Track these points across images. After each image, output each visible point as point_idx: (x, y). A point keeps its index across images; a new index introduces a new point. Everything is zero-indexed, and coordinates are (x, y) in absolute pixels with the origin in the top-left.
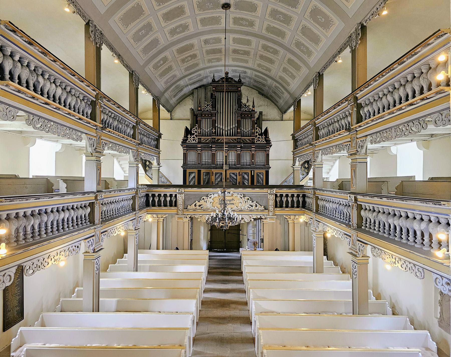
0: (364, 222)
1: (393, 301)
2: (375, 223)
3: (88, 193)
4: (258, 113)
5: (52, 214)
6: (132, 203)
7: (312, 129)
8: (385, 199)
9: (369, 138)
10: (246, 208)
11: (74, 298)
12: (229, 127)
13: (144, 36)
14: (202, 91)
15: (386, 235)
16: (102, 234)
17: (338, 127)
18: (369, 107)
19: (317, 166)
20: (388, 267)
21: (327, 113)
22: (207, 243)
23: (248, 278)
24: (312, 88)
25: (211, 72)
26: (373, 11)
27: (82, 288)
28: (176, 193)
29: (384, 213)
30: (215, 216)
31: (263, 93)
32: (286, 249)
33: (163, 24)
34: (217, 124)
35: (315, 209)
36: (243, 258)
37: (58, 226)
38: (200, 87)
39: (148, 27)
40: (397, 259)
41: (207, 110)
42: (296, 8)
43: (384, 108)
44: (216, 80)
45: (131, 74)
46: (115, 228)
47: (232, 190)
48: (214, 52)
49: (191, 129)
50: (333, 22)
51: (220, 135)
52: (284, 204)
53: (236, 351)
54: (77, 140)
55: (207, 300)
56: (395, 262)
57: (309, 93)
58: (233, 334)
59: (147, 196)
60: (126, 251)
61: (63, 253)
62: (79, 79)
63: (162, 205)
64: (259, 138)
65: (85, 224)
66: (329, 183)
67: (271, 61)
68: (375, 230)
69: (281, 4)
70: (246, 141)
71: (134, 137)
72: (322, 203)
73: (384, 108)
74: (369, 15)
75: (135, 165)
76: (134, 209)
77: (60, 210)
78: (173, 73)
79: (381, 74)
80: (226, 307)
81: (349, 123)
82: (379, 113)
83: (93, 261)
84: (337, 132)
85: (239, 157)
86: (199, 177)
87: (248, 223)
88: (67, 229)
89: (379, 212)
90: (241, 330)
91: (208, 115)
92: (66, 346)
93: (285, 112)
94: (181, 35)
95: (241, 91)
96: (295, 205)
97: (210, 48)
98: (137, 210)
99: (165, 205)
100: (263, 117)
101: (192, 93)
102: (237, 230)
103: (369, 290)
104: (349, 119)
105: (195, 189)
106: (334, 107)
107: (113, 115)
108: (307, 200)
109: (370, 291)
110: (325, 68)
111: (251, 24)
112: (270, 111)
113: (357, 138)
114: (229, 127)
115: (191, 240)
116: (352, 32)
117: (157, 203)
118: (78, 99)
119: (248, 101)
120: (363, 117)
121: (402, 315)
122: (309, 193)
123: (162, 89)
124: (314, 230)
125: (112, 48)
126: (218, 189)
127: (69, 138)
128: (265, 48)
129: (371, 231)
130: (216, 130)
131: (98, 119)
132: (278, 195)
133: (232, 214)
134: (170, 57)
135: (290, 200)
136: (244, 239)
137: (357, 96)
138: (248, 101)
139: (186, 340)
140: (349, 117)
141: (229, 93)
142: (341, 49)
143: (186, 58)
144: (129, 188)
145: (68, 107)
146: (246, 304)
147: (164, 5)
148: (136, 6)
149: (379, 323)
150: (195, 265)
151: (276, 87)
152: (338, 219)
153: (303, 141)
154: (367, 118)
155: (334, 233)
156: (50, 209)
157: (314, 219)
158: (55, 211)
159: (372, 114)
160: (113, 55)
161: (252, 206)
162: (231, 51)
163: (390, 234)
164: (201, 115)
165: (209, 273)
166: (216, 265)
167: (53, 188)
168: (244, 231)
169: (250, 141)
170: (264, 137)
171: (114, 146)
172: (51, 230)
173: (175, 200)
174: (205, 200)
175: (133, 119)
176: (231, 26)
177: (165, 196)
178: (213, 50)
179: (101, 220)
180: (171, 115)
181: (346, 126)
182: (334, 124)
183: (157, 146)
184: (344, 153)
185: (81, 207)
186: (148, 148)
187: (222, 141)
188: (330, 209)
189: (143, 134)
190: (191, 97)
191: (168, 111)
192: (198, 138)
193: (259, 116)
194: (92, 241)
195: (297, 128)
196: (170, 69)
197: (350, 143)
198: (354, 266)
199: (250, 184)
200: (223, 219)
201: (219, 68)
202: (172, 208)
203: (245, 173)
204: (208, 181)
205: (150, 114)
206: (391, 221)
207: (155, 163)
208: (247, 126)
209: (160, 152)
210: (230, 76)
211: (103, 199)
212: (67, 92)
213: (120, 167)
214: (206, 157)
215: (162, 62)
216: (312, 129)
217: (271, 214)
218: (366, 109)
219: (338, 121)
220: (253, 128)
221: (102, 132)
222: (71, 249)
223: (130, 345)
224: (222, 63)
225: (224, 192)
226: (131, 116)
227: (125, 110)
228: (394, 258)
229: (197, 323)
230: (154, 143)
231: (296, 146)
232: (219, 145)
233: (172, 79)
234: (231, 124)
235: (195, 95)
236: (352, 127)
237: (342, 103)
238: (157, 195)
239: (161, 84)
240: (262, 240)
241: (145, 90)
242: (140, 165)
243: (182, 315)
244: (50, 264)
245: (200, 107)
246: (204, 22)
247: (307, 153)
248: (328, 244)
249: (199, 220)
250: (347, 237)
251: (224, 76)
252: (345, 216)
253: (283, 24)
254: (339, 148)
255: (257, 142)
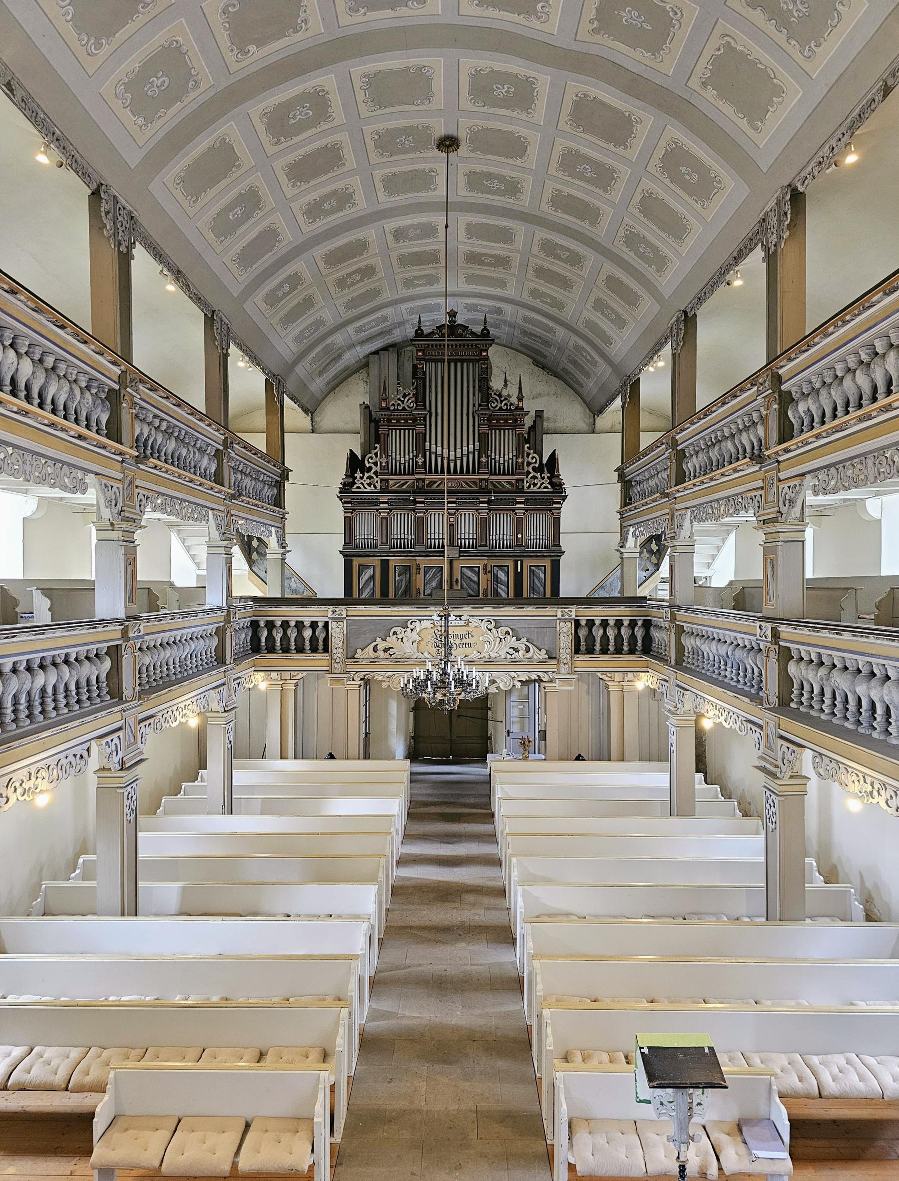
0: (796, 692)
1: (869, 885)
2: (822, 693)
3: (105, 622)
4: (532, 413)
5: (14, 678)
6: (215, 644)
7: (667, 455)
8: (847, 636)
9: (809, 481)
10: (503, 654)
11: (75, 881)
12: (459, 451)
13: (240, 222)
14: (390, 359)
15: (849, 725)
16: (142, 725)
17: (733, 450)
18: (810, 401)
19: (679, 549)
20: (854, 806)
21: (706, 415)
22: (406, 741)
23: (507, 830)
24: (667, 350)
25: (411, 312)
26: (821, 154)
27: (93, 857)
28: (326, 619)
29: (846, 668)
30: (422, 677)
31: (543, 364)
32: (603, 755)
33: (290, 192)
34: (427, 444)
35: (673, 656)
36: (496, 779)
37: (30, 707)
38: (385, 349)
39: (251, 201)
40: (877, 786)
41: (404, 409)
42: (626, 148)
43: (847, 404)
44: (426, 330)
45: (210, 320)
46: (175, 708)
47: (466, 611)
48: (420, 259)
49: (364, 457)
50: (720, 182)
51: (436, 472)
52: (598, 644)
53: (478, 1012)
54: (74, 490)
55: (408, 883)
56: (871, 793)
57: (661, 364)
58: (468, 968)
59: (254, 625)
60: (203, 765)
61: (43, 773)
62: (75, 335)
63: (293, 647)
64: (534, 477)
65: (99, 700)
66: (711, 591)
67: (565, 283)
68: (822, 710)
69: (587, 137)
70: (503, 486)
71: (218, 478)
72: (693, 642)
73: (847, 404)
74: (812, 164)
75: (222, 550)
76: (220, 660)
77: (36, 666)
78: (317, 316)
79: (839, 317)
80: (454, 902)
81: (760, 441)
82: (835, 416)
83: (119, 791)
84: (731, 463)
85: (484, 526)
86: (384, 578)
87: (508, 693)
88: (54, 714)
89: (834, 666)
90: (485, 957)
91: (406, 421)
92: (57, 1002)
93: (601, 411)
94: (333, 217)
95: (488, 359)
96: (626, 648)
97: (410, 250)
98: (228, 661)
99: (300, 650)
100: (545, 424)
101: (364, 365)
102: (480, 709)
103: (807, 860)
104: (760, 430)
105: (373, 608)
106: (722, 401)
107: (164, 424)
108: (655, 634)
109: (811, 861)
110: (700, 299)
111: (513, 188)
112: (563, 410)
113: (780, 481)
114: (459, 451)
115: (366, 734)
116: (768, 208)
117: (278, 644)
118: (74, 386)
119: (506, 385)
120: (796, 426)
121: (890, 921)
122: (661, 617)
123: (288, 356)
124: (673, 709)
125: (158, 255)
126: (432, 608)
127: (53, 486)
128: (549, 248)
129: (813, 713)
130: (425, 457)
131: (126, 436)
132: (583, 623)
133: (465, 670)
134: (307, 275)
135: (611, 633)
136: (497, 731)
137: (780, 372)
138: (506, 385)
139: (353, 986)
140: (759, 426)
141: (459, 364)
142: (741, 250)
143: (349, 275)
144: (207, 607)
145: (49, 407)
146: (502, 892)
147: (290, 143)
148: (218, 145)
149: (825, 942)
150: (375, 800)
151: (577, 347)
152: (733, 683)
153: (645, 486)
154: (805, 429)
155: (722, 719)
156: (10, 666)
157: (673, 682)
158: (22, 668)
159: (816, 420)
160: (162, 271)
161: (516, 650)
162: (462, 258)
163: (859, 723)
164: (389, 421)
165: (410, 816)
166: (430, 795)
167: (17, 610)
168: (498, 712)
169: (512, 485)
170: (546, 475)
171: (169, 503)
172: (13, 717)
173: (323, 635)
174: (400, 636)
175: (216, 433)
176: (462, 193)
177: (300, 625)
178: (416, 254)
179: (138, 688)
180: (312, 419)
181: (753, 448)
182: (723, 444)
183: (279, 501)
184: (749, 516)
185: (87, 658)
186: (256, 505)
187: (441, 487)
188: (711, 658)
189: (242, 472)
190: (363, 374)
191: (306, 411)
192: (382, 480)
193: (535, 422)
194: (116, 741)
195: (631, 452)
196: (308, 303)
197: (762, 492)
198: (770, 801)
199: (511, 595)
200: (443, 683)
201: (433, 301)
202: (318, 656)
203: (500, 567)
204: (406, 586)
205: (260, 419)
206: (861, 689)
207: (273, 542)
208: (504, 449)
209: (287, 516)
210: (460, 320)
211: (142, 637)
212: (46, 370)
213: (183, 555)
214: (401, 527)
215: (287, 288)
216: (667, 455)
217: (564, 669)
218: (802, 407)
219: (733, 435)
220: (520, 452)
221: (138, 468)
222: (64, 762)
223: (215, 999)
224: (440, 287)
225: (447, 617)
226: (209, 425)
227: (194, 411)
228: (869, 782)
229: (381, 942)
230: (270, 493)
231: (627, 499)
232: (430, 495)
233: (314, 332)
234: (465, 444)
235: (374, 370)
236: (767, 453)
237: (743, 390)
238: (278, 624)
239: (285, 343)
240: (543, 735)
241: (247, 358)
242: (236, 551)
243: (344, 921)
244: (13, 800)
245: (384, 400)
246: (392, 184)
247: (654, 514)
248: (707, 743)
249: (384, 685)
250: (754, 728)
251: (444, 320)
252: (749, 675)
253: (594, 189)
254: (735, 503)
255: (529, 487)
